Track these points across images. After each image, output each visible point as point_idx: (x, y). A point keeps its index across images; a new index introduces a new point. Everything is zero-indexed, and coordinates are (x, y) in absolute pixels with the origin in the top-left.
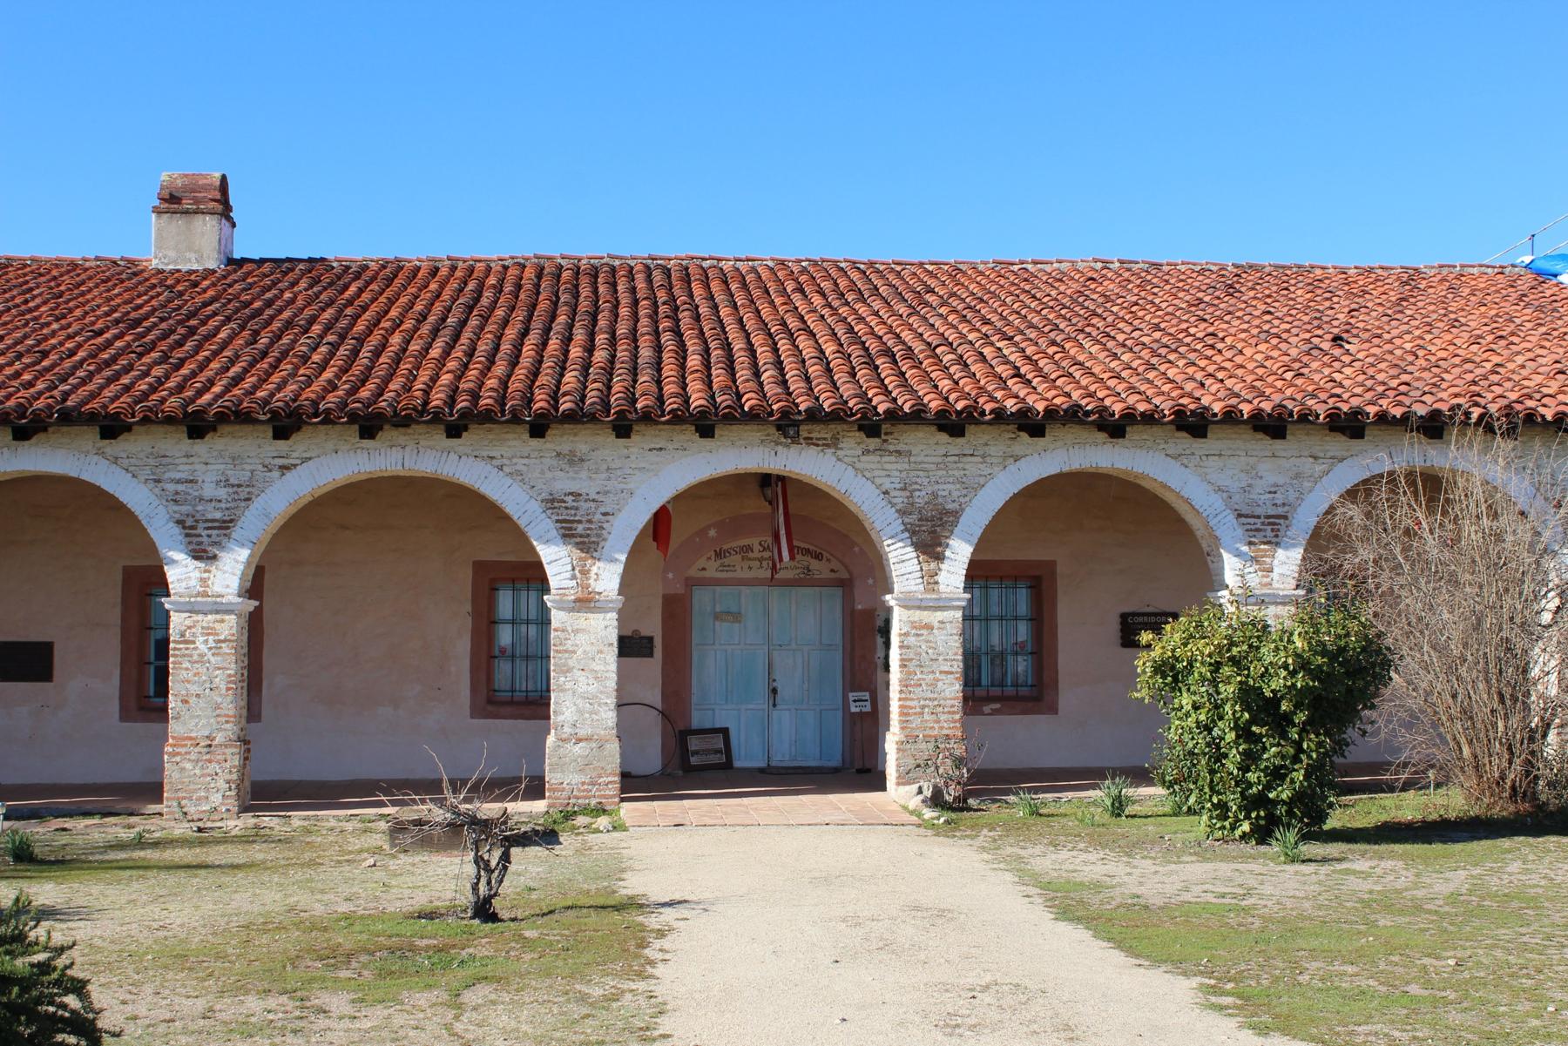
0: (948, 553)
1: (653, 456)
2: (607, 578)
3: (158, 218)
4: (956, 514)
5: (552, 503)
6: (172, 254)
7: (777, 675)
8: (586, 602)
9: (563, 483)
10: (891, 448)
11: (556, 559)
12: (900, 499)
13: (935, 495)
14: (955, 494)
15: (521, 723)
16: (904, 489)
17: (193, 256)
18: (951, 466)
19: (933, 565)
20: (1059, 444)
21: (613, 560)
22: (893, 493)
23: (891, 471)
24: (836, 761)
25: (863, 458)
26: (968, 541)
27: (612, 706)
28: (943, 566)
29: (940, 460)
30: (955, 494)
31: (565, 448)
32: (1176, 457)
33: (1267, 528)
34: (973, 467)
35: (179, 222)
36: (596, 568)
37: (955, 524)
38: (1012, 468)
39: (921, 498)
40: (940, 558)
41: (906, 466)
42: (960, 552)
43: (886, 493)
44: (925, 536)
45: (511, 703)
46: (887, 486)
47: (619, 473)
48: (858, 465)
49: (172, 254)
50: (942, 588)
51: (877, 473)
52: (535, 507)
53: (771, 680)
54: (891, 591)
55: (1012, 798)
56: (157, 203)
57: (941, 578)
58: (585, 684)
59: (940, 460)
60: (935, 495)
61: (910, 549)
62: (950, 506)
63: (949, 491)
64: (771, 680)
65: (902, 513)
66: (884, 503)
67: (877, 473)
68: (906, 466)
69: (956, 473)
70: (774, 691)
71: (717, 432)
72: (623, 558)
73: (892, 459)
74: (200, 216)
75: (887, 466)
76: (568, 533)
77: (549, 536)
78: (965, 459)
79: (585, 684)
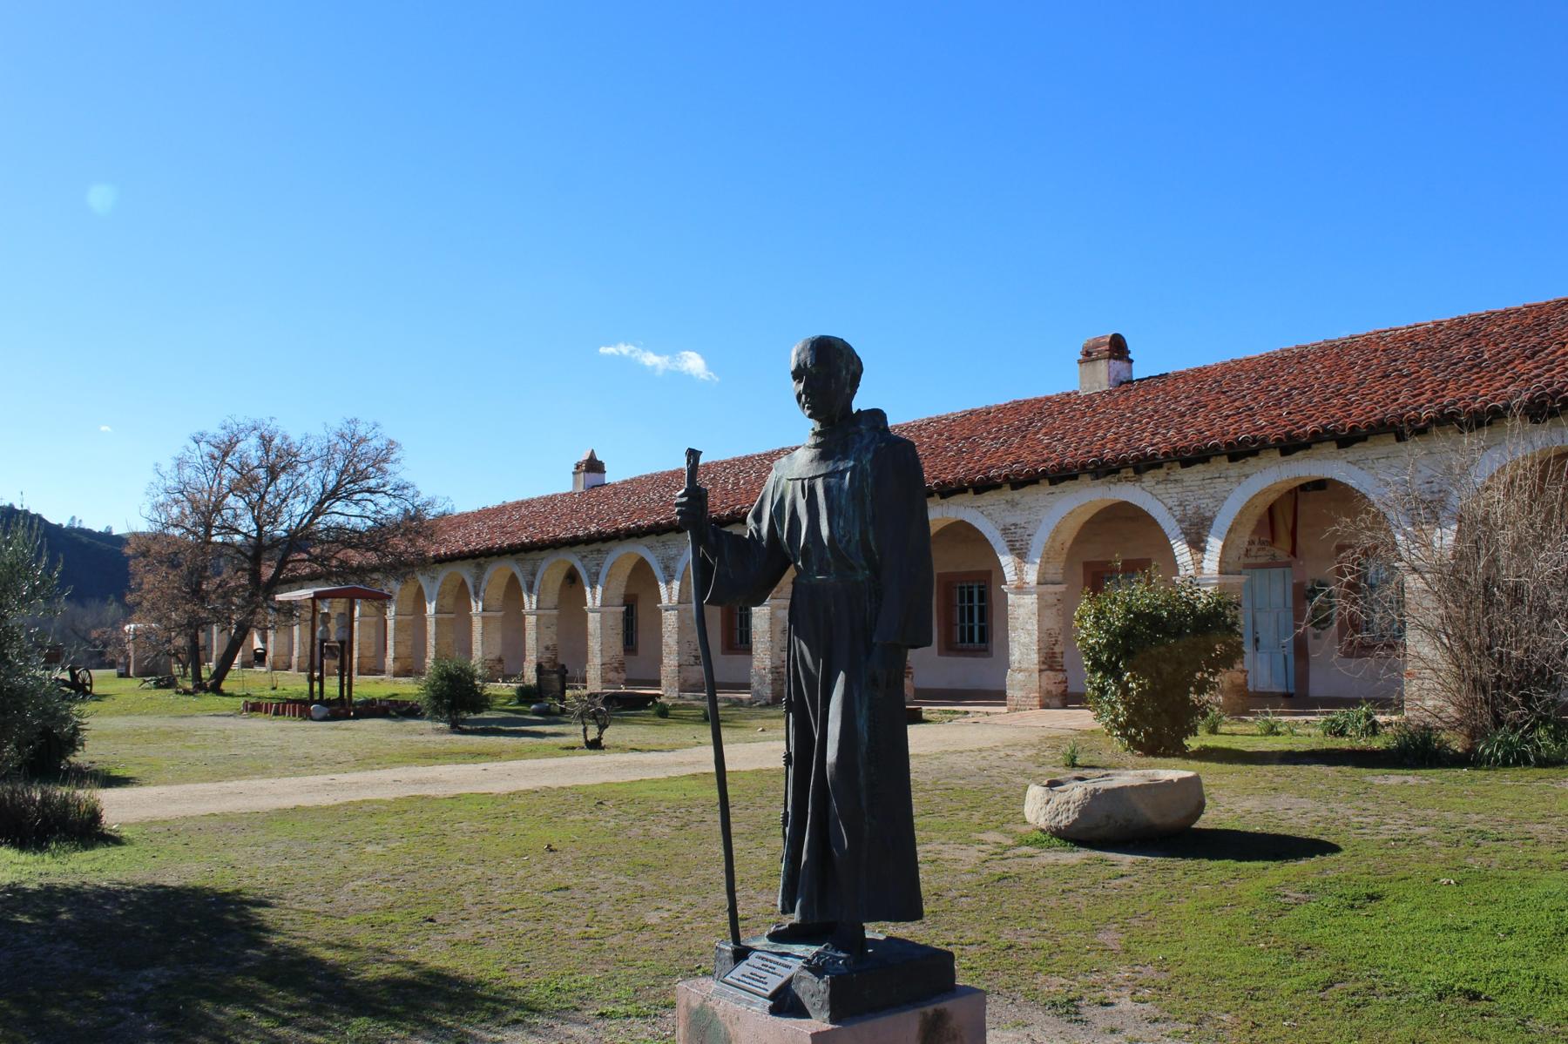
1: (1050, 498)
2: (1031, 574)
4: (1211, 519)
5: (1005, 530)
7: (1259, 629)
8: (1021, 589)
9: (1010, 519)
11: (1007, 562)
12: (1178, 512)
13: (1198, 507)
23: (1172, 493)
24: (1279, 689)
31: (1009, 498)
32: (1354, 463)
33: (1431, 509)
34: (1220, 485)
35: (1090, 366)
36: (1027, 567)
37: (1210, 526)
38: (1245, 483)
39: (1190, 511)
40: (1203, 550)
42: (1215, 545)
46: (1170, 504)
52: (998, 533)
53: (1255, 632)
54: (1005, 583)
55: (1251, 719)
58: (1024, 638)
60: (1198, 507)
62: (1208, 514)
63: (1206, 503)
64: (1255, 632)
65: (1180, 521)
70: (1257, 640)
76: (1012, 550)
79: (1024, 638)
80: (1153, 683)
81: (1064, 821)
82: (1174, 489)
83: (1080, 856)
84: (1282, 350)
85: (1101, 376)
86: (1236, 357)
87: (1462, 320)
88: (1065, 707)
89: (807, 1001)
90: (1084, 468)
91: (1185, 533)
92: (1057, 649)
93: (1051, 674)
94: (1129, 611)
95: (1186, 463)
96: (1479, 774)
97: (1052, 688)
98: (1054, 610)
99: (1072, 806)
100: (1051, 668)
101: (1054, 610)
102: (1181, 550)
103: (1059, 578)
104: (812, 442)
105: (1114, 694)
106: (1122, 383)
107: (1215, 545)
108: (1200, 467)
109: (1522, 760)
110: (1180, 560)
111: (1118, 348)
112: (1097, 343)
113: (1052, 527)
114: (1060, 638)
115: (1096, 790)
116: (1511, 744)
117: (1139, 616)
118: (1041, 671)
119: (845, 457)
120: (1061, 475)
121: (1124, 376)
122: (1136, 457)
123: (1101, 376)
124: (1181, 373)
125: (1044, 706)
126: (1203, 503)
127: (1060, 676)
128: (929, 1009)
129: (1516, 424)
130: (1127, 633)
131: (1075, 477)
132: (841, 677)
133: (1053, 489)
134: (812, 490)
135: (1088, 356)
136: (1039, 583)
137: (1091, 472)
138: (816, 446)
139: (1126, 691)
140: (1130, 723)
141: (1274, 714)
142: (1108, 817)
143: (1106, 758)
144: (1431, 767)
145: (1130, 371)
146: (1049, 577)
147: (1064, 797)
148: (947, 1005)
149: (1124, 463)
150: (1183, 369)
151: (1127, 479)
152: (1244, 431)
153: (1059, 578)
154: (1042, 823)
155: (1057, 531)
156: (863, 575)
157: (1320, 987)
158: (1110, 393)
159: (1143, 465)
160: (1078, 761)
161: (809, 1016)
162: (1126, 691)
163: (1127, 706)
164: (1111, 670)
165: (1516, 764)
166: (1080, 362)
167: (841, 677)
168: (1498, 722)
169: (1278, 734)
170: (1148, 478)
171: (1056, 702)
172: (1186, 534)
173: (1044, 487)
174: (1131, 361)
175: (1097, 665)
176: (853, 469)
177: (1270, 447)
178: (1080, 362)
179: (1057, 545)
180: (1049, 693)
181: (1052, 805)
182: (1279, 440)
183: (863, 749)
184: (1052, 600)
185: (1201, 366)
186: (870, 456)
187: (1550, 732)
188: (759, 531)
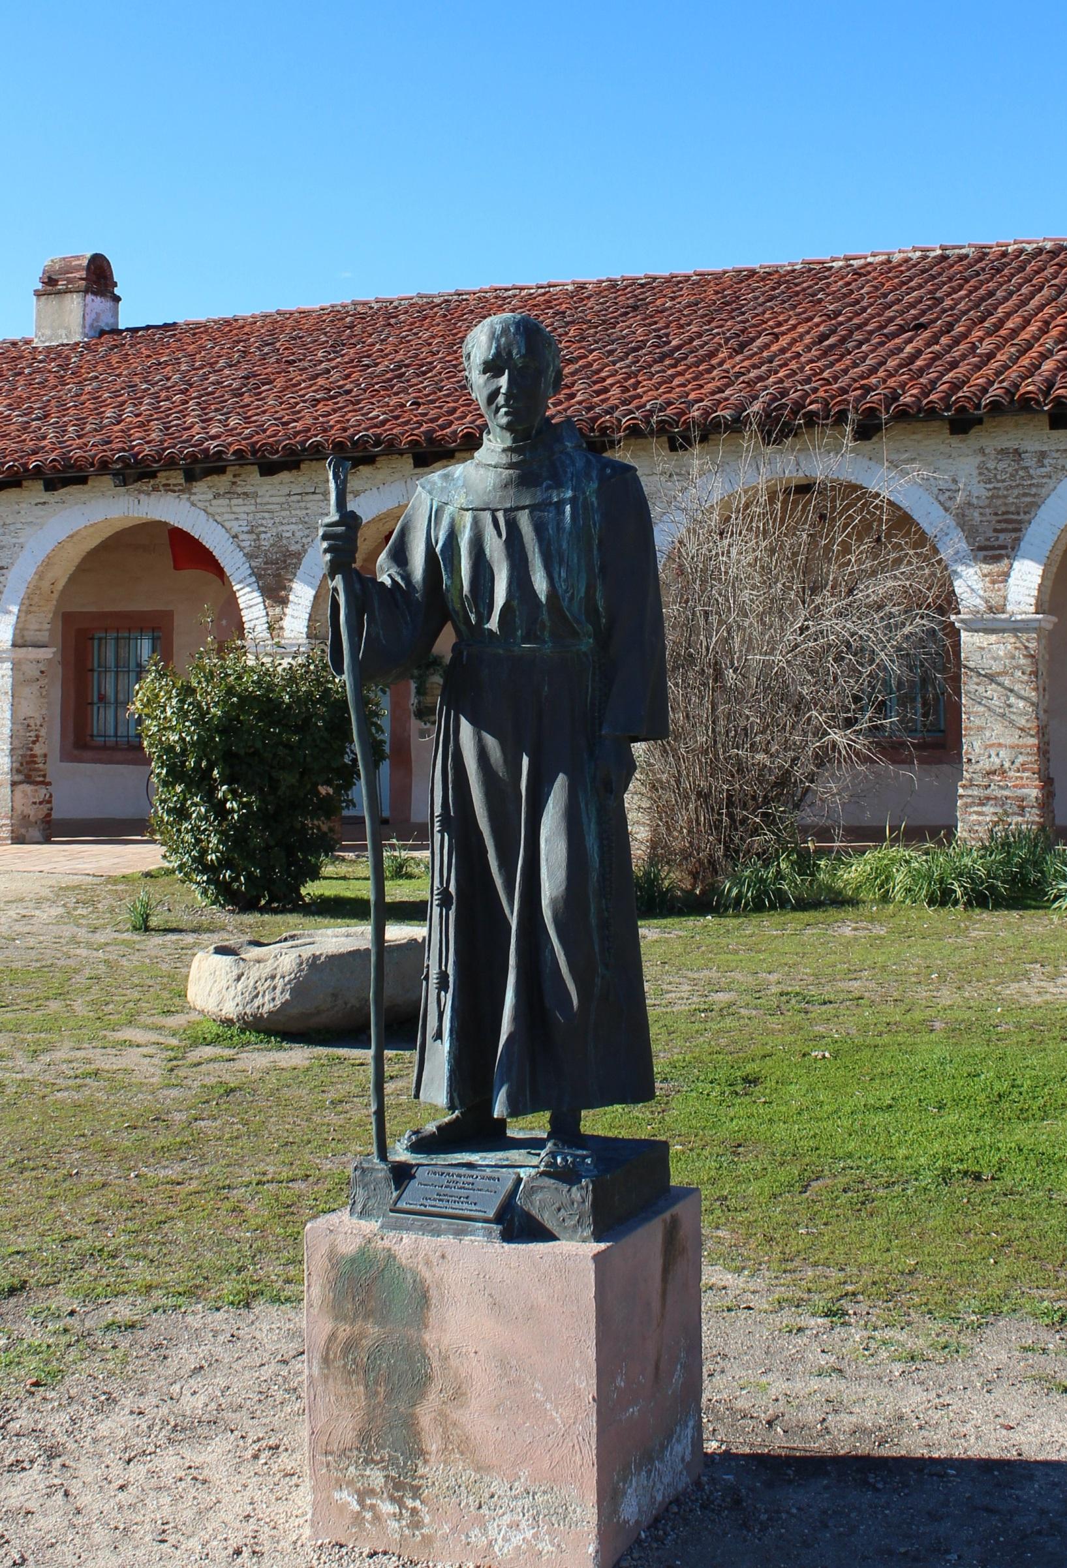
0: (291, 597)
1: (39, 511)
3: (38, 300)
4: (299, 556)
6: (48, 332)
10: (239, 490)
12: (247, 542)
13: (279, 537)
14: (299, 534)
15: (100, 768)
16: (250, 532)
17: (63, 332)
18: (294, 505)
19: (278, 610)
20: (396, 476)
21: (8, 612)
22: (241, 537)
25: (214, 502)
26: (310, 584)
27: (7, 752)
28: (287, 611)
29: (283, 500)
30: (299, 534)
35: (53, 302)
37: (297, 566)
39: (266, 541)
40: (284, 602)
41: (253, 508)
43: (235, 537)
44: (270, 580)
45: (115, 748)
47: (12, 528)
48: (210, 510)
49: (48, 332)
50: (287, 634)
51: (226, 516)
56: (40, 286)
57: (286, 623)
59: (283, 500)
60: (279, 537)
61: (256, 594)
65: (249, 556)
66: (233, 547)
67: (226, 516)
68: (253, 508)
69: (298, 512)
71: (25, 483)
72: (15, 609)
73: (240, 501)
74: (69, 295)
75: (235, 509)
77: (313, 581)
78: (307, 498)
79: (997, 731)
80: (263, 799)
81: (267, 1004)
82: (243, 508)
83: (298, 1056)
84: (355, 303)
85: (71, 320)
86: (284, 308)
87: (613, 285)
88: (47, 840)
89: (548, 1220)
90: (104, 467)
91: (257, 574)
92: (38, 749)
93: (28, 788)
94: (230, 691)
95: (269, 469)
96: (731, 922)
97: (31, 811)
98: (35, 687)
99: (280, 983)
100: (28, 780)
101: (35, 687)
102: (251, 605)
103: (44, 637)
104: (504, 459)
105: (200, 818)
106: (102, 333)
107: (302, 595)
108: (285, 476)
109: (780, 903)
110: (246, 615)
111: (98, 277)
112: (67, 267)
113: (41, 557)
114: (43, 732)
115: (315, 957)
116: (762, 880)
117: (246, 700)
118: (14, 784)
119: (559, 485)
120: (64, 476)
121: (105, 323)
122: (192, 455)
123: (71, 320)
124: (198, 325)
125: (18, 839)
126: (287, 530)
127: (42, 792)
128: (667, 1215)
129: (749, 441)
130: (228, 727)
131: (83, 481)
132: (561, 781)
133: (46, 496)
134: (512, 526)
135: (52, 285)
136: (14, 645)
137: (116, 474)
138: (511, 466)
139: (220, 810)
140: (225, 862)
141: (404, 847)
142: (335, 996)
143: (184, 919)
144: (663, 916)
145: (115, 314)
146: (30, 636)
147: (266, 969)
148: (677, 1209)
149: (171, 463)
150: (202, 319)
151: (168, 488)
152: (356, 423)
153: (44, 637)
154: (230, 1009)
155: (48, 563)
156: (587, 644)
157: (797, 1187)
158: (87, 346)
159: (200, 467)
160: (154, 922)
161: (553, 1238)
162: (220, 810)
163: (224, 836)
164: (200, 782)
165: (773, 907)
166: (38, 294)
167: (561, 781)
168: (732, 853)
169: (410, 876)
170: (202, 489)
171: (35, 833)
172: (259, 577)
173: (35, 491)
174: (117, 299)
175: (176, 774)
176: (573, 501)
177: (401, 453)
178: (38, 294)
179: (45, 585)
180: (25, 817)
181: (247, 982)
182: (414, 444)
183: (594, 876)
184: (32, 671)
185: (228, 315)
186: (594, 485)
187: (793, 863)
188: (407, 577)
